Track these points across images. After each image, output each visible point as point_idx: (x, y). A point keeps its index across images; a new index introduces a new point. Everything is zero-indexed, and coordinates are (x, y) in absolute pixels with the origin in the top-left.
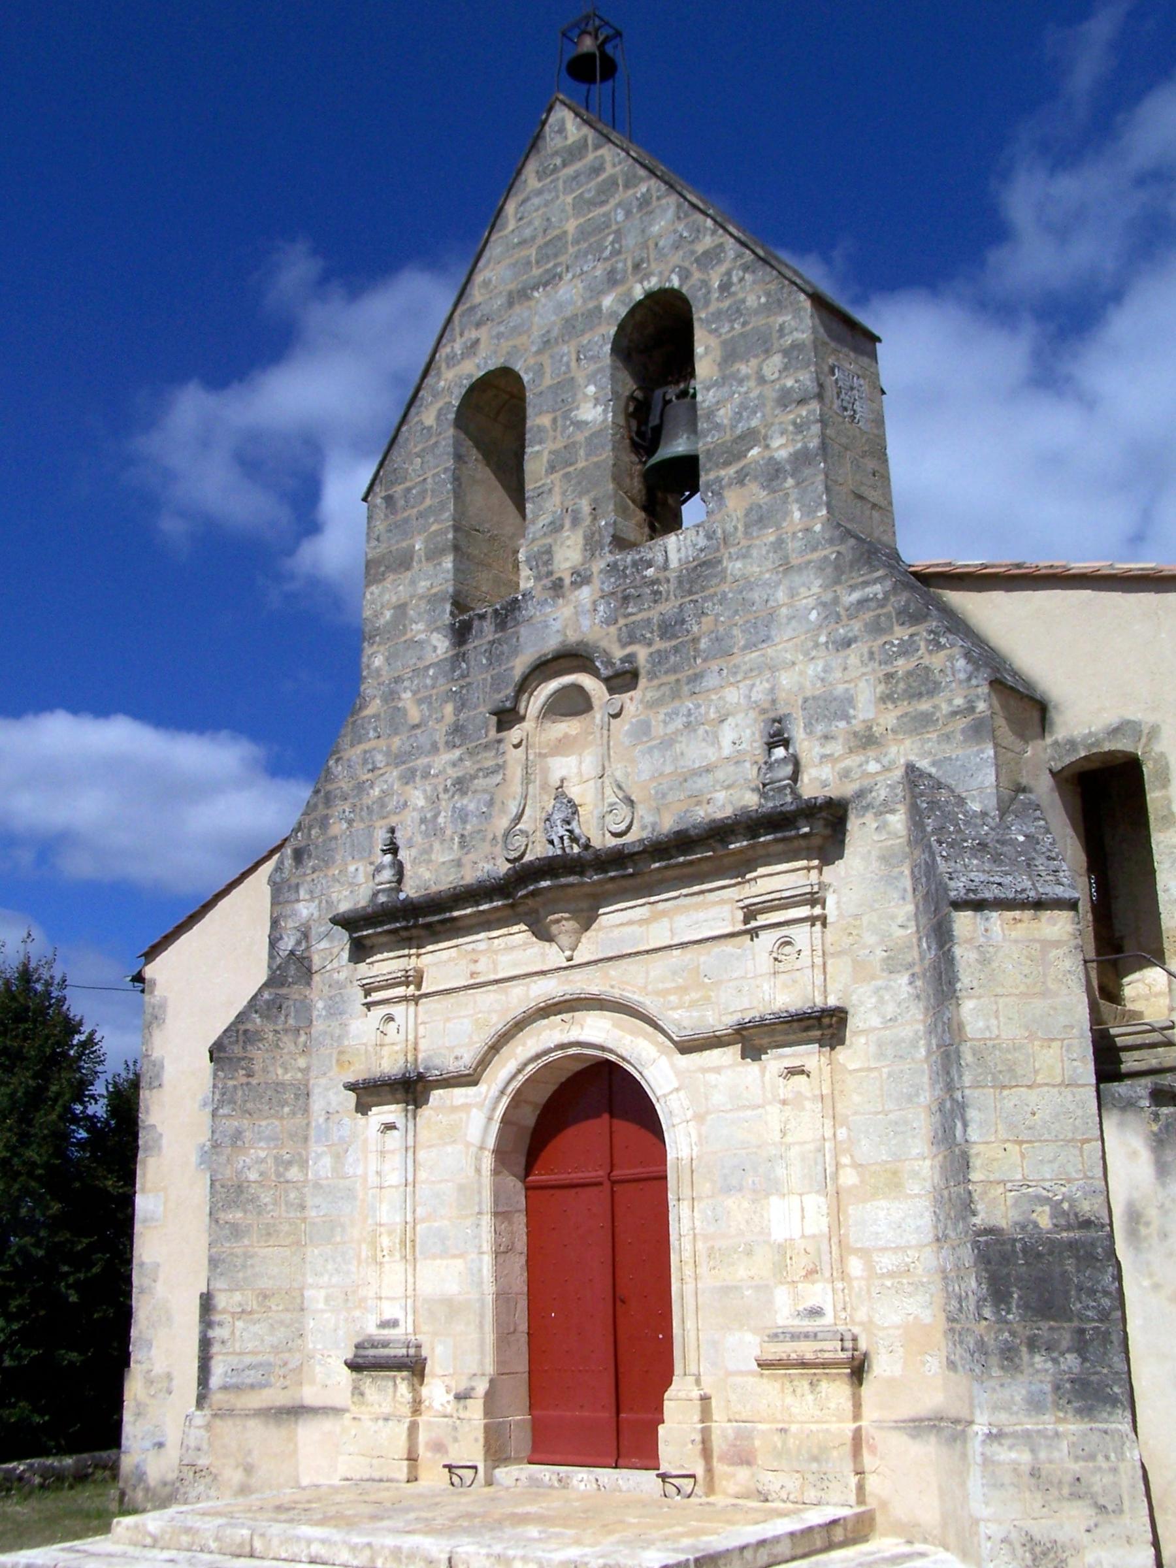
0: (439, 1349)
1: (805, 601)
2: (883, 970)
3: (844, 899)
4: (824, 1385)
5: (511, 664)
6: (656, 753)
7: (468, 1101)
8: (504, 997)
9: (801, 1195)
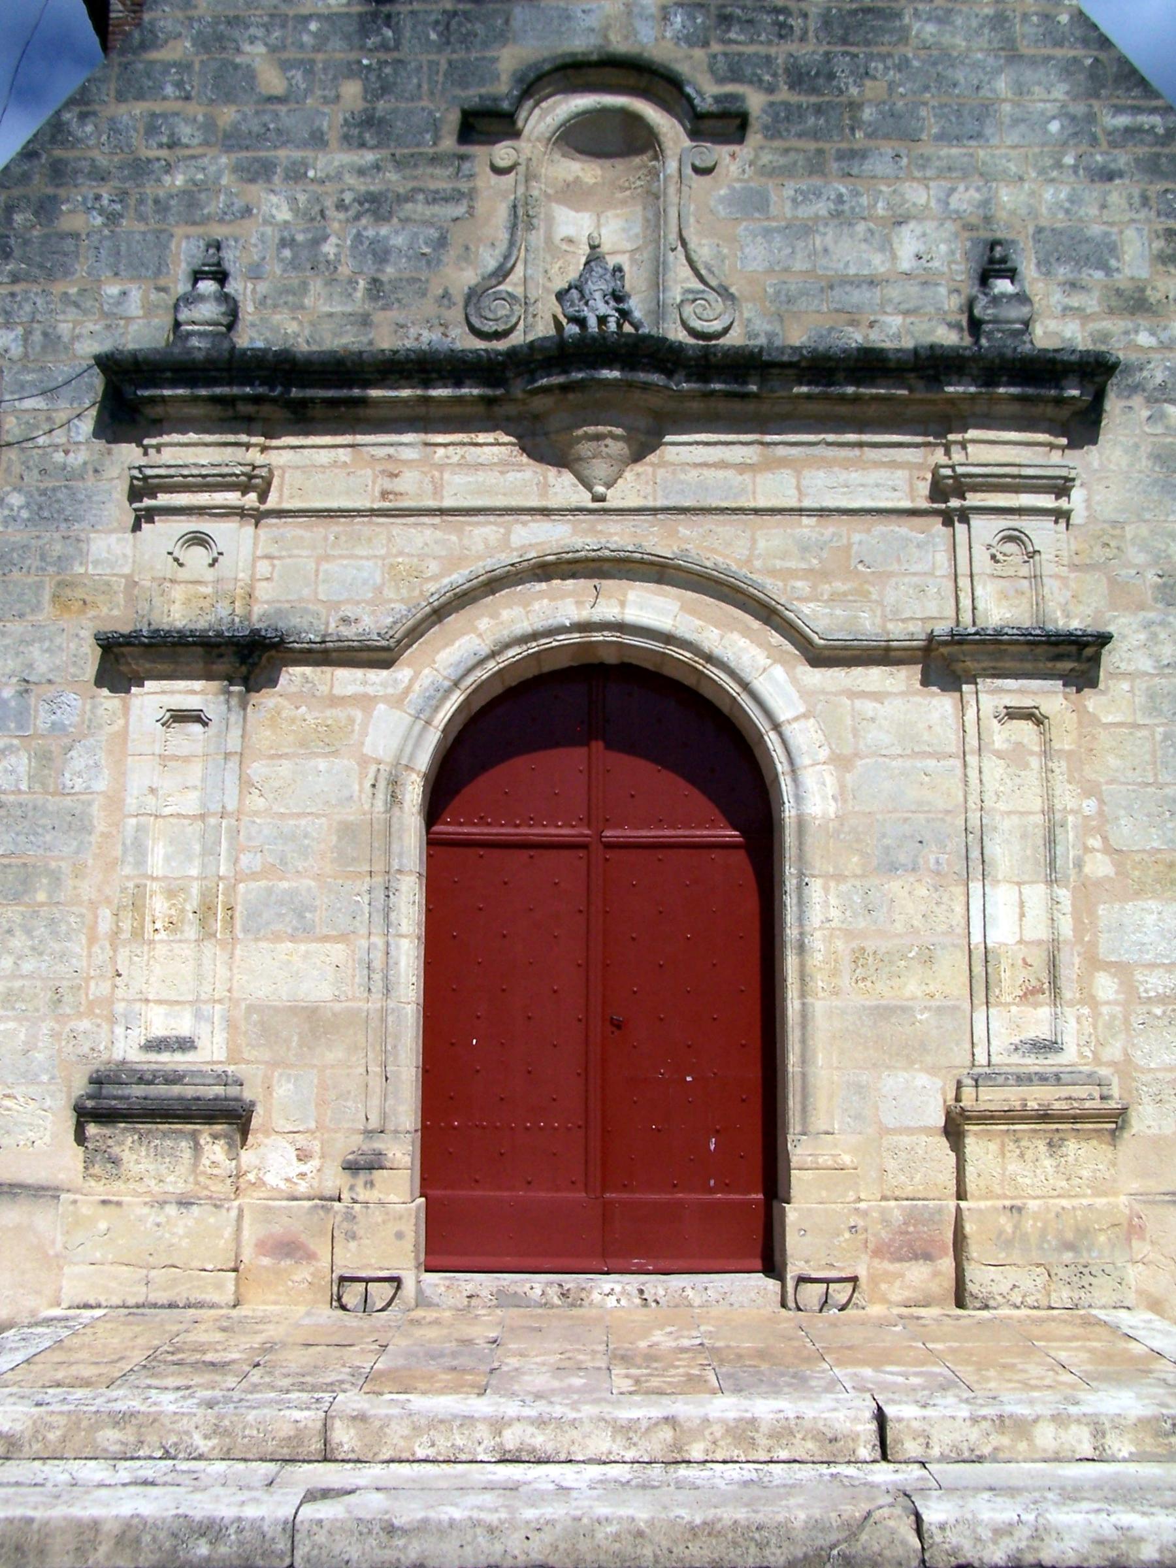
0: (283, 1090)
1: (1041, 105)
2: (1156, 600)
3: (1097, 498)
4: (1071, 1146)
5: (489, 54)
6: (778, 240)
7: (370, 690)
8: (454, 538)
9: (1019, 884)
